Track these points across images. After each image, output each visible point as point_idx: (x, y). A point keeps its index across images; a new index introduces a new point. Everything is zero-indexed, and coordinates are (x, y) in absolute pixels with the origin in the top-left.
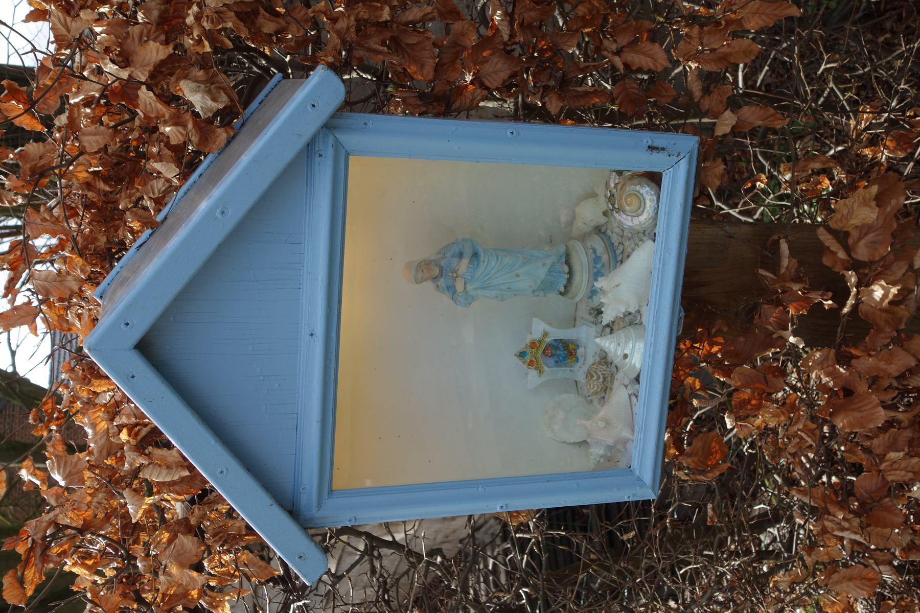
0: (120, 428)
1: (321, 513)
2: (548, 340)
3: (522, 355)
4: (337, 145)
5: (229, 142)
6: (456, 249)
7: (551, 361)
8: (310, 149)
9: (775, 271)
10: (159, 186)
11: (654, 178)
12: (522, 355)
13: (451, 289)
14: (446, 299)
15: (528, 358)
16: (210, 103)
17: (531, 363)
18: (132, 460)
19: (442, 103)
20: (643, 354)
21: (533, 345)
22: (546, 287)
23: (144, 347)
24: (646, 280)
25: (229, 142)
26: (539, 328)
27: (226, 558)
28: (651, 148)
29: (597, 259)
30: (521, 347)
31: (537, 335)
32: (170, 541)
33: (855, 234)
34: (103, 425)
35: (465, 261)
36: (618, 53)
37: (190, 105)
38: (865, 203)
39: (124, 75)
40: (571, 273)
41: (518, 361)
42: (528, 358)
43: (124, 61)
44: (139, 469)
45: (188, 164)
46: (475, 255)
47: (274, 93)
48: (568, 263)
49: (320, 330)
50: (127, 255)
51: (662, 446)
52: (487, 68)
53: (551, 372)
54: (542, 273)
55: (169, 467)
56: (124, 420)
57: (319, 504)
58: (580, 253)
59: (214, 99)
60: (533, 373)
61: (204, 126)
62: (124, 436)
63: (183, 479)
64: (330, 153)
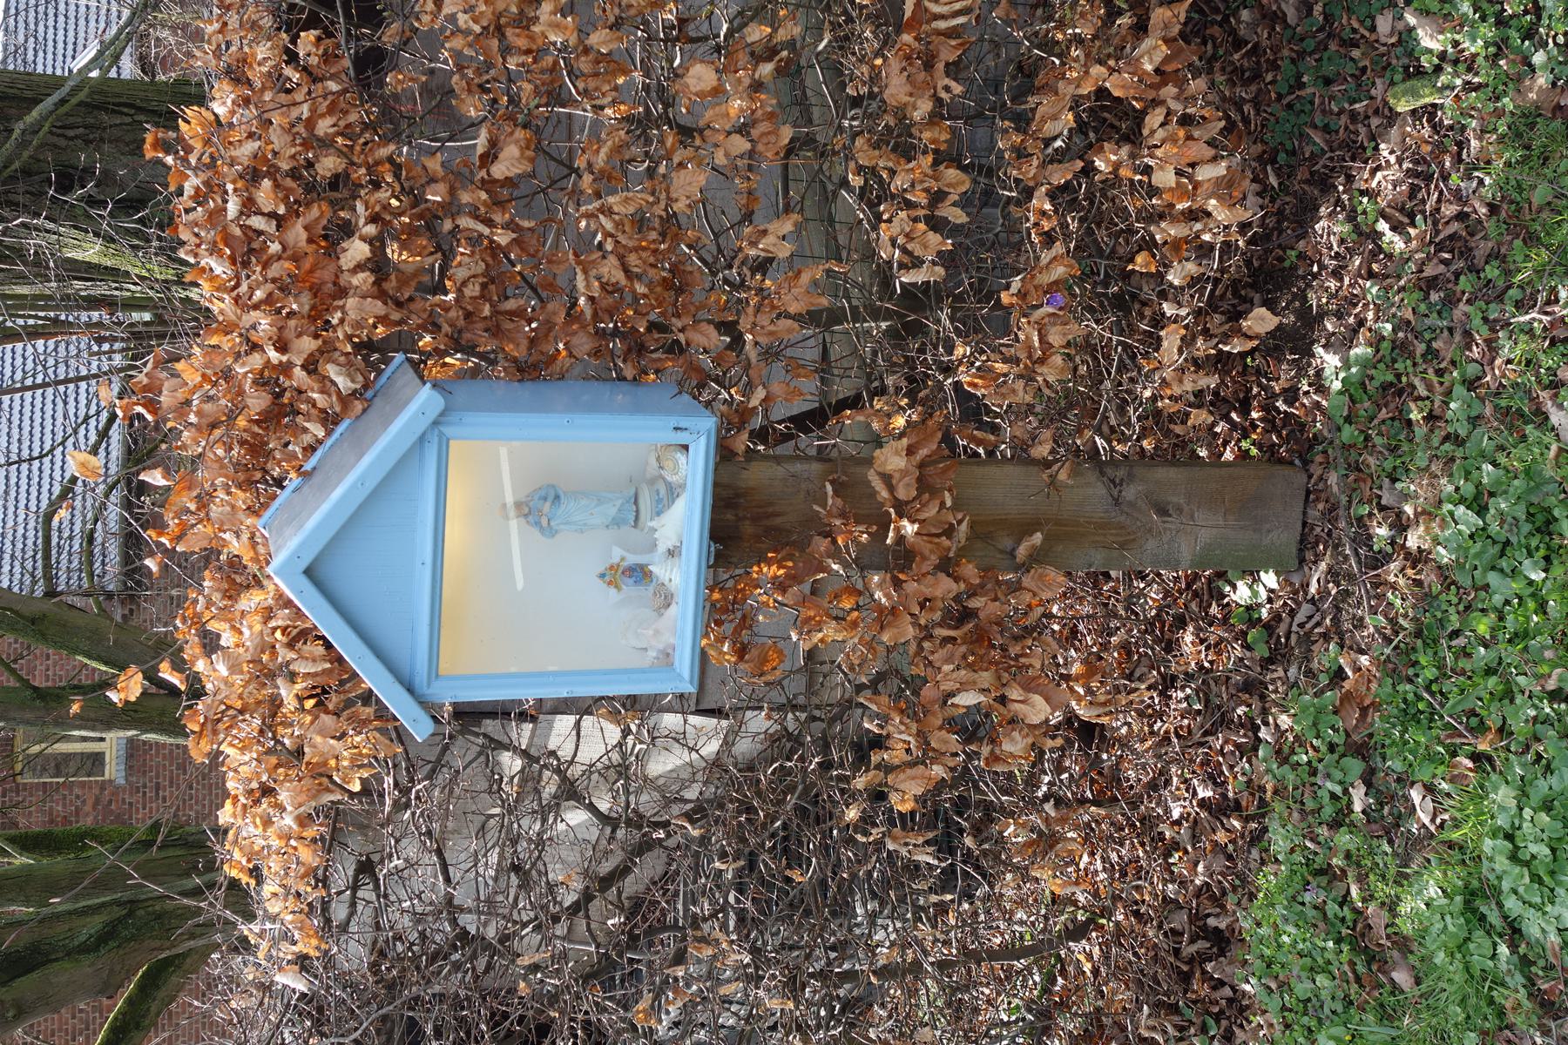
0: (274, 629)
1: (430, 691)
2: (625, 564)
3: (602, 576)
4: (441, 434)
5: (364, 410)
6: (543, 493)
7: (631, 581)
8: (422, 439)
9: (824, 506)
10: (307, 439)
11: (686, 447)
12: (602, 576)
13: (538, 524)
14: (535, 532)
15: (607, 578)
16: (350, 384)
17: (610, 583)
18: (284, 654)
19: (532, 369)
20: (683, 576)
21: (611, 567)
22: (617, 522)
23: (309, 572)
24: (683, 523)
25: (364, 410)
26: (616, 554)
27: (358, 739)
28: (676, 429)
29: (659, 501)
30: (601, 569)
31: (615, 560)
32: (312, 723)
33: (897, 475)
34: (258, 627)
35: (548, 504)
36: (682, 330)
37: (333, 383)
38: (897, 453)
39: (284, 358)
40: (637, 511)
41: (598, 581)
42: (607, 578)
43: (282, 347)
44: (288, 663)
45: (330, 421)
46: (557, 497)
47: (398, 374)
48: (636, 503)
49: (429, 561)
50: (283, 496)
51: (698, 650)
52: (575, 341)
53: (629, 589)
54: (613, 511)
55: (314, 661)
56: (280, 623)
57: (429, 685)
58: (639, 499)
59: (353, 381)
60: (612, 591)
61: (345, 400)
62: (278, 634)
63: (324, 671)
64: (436, 439)
